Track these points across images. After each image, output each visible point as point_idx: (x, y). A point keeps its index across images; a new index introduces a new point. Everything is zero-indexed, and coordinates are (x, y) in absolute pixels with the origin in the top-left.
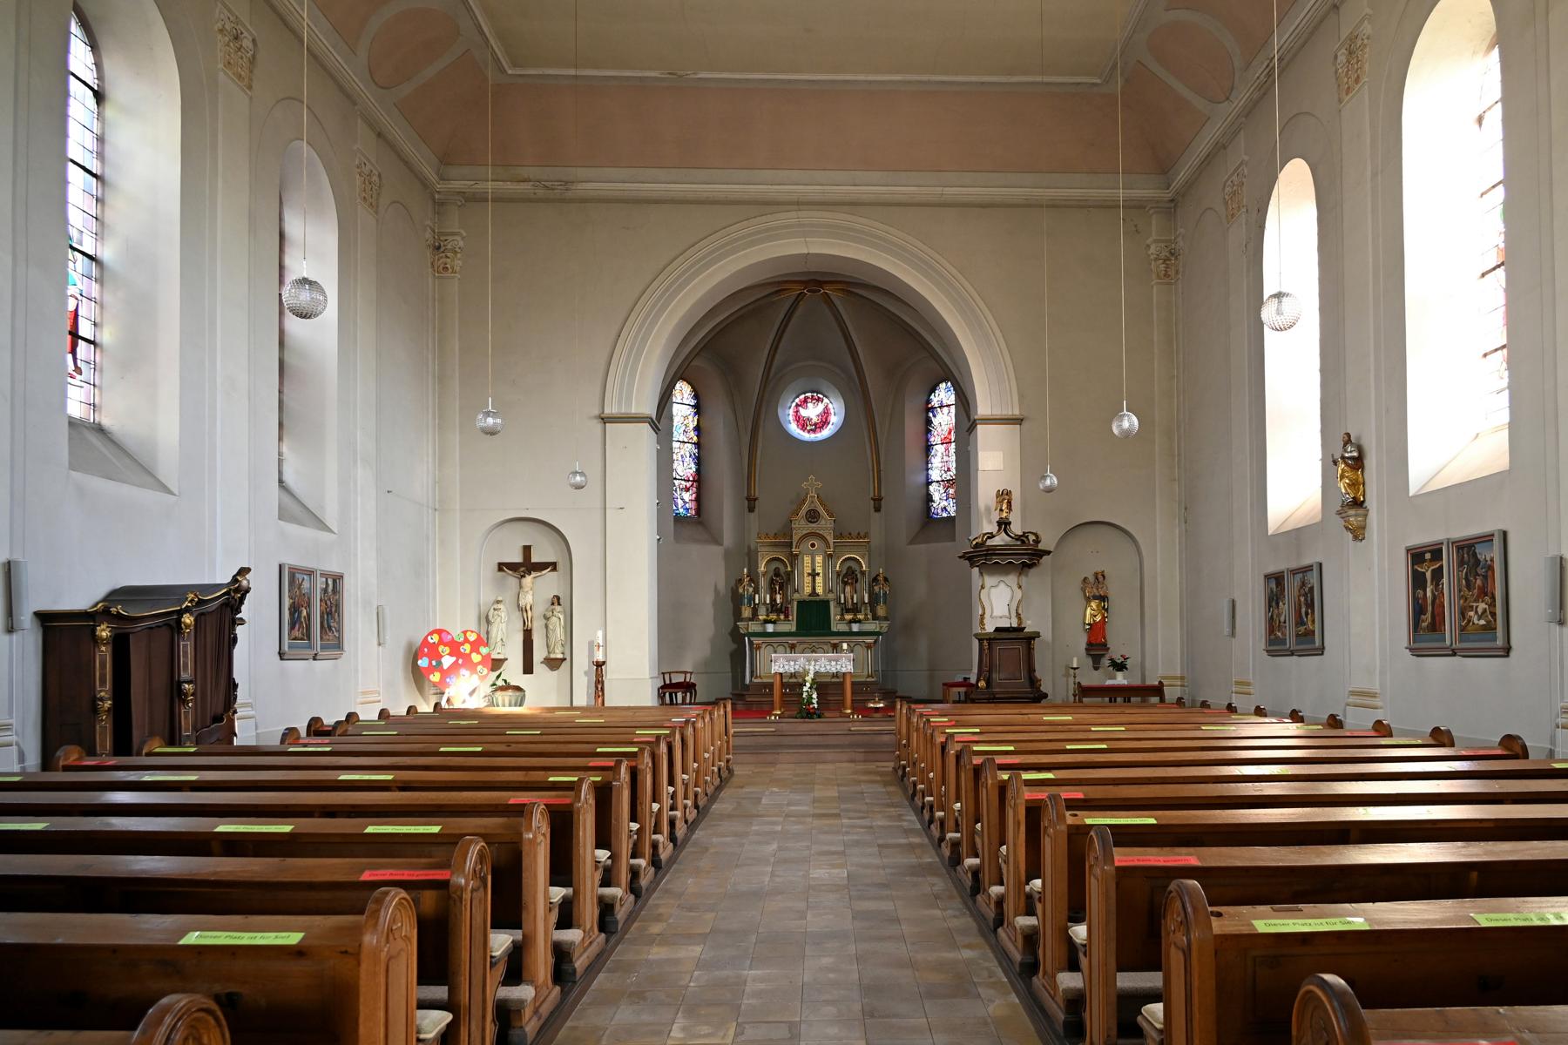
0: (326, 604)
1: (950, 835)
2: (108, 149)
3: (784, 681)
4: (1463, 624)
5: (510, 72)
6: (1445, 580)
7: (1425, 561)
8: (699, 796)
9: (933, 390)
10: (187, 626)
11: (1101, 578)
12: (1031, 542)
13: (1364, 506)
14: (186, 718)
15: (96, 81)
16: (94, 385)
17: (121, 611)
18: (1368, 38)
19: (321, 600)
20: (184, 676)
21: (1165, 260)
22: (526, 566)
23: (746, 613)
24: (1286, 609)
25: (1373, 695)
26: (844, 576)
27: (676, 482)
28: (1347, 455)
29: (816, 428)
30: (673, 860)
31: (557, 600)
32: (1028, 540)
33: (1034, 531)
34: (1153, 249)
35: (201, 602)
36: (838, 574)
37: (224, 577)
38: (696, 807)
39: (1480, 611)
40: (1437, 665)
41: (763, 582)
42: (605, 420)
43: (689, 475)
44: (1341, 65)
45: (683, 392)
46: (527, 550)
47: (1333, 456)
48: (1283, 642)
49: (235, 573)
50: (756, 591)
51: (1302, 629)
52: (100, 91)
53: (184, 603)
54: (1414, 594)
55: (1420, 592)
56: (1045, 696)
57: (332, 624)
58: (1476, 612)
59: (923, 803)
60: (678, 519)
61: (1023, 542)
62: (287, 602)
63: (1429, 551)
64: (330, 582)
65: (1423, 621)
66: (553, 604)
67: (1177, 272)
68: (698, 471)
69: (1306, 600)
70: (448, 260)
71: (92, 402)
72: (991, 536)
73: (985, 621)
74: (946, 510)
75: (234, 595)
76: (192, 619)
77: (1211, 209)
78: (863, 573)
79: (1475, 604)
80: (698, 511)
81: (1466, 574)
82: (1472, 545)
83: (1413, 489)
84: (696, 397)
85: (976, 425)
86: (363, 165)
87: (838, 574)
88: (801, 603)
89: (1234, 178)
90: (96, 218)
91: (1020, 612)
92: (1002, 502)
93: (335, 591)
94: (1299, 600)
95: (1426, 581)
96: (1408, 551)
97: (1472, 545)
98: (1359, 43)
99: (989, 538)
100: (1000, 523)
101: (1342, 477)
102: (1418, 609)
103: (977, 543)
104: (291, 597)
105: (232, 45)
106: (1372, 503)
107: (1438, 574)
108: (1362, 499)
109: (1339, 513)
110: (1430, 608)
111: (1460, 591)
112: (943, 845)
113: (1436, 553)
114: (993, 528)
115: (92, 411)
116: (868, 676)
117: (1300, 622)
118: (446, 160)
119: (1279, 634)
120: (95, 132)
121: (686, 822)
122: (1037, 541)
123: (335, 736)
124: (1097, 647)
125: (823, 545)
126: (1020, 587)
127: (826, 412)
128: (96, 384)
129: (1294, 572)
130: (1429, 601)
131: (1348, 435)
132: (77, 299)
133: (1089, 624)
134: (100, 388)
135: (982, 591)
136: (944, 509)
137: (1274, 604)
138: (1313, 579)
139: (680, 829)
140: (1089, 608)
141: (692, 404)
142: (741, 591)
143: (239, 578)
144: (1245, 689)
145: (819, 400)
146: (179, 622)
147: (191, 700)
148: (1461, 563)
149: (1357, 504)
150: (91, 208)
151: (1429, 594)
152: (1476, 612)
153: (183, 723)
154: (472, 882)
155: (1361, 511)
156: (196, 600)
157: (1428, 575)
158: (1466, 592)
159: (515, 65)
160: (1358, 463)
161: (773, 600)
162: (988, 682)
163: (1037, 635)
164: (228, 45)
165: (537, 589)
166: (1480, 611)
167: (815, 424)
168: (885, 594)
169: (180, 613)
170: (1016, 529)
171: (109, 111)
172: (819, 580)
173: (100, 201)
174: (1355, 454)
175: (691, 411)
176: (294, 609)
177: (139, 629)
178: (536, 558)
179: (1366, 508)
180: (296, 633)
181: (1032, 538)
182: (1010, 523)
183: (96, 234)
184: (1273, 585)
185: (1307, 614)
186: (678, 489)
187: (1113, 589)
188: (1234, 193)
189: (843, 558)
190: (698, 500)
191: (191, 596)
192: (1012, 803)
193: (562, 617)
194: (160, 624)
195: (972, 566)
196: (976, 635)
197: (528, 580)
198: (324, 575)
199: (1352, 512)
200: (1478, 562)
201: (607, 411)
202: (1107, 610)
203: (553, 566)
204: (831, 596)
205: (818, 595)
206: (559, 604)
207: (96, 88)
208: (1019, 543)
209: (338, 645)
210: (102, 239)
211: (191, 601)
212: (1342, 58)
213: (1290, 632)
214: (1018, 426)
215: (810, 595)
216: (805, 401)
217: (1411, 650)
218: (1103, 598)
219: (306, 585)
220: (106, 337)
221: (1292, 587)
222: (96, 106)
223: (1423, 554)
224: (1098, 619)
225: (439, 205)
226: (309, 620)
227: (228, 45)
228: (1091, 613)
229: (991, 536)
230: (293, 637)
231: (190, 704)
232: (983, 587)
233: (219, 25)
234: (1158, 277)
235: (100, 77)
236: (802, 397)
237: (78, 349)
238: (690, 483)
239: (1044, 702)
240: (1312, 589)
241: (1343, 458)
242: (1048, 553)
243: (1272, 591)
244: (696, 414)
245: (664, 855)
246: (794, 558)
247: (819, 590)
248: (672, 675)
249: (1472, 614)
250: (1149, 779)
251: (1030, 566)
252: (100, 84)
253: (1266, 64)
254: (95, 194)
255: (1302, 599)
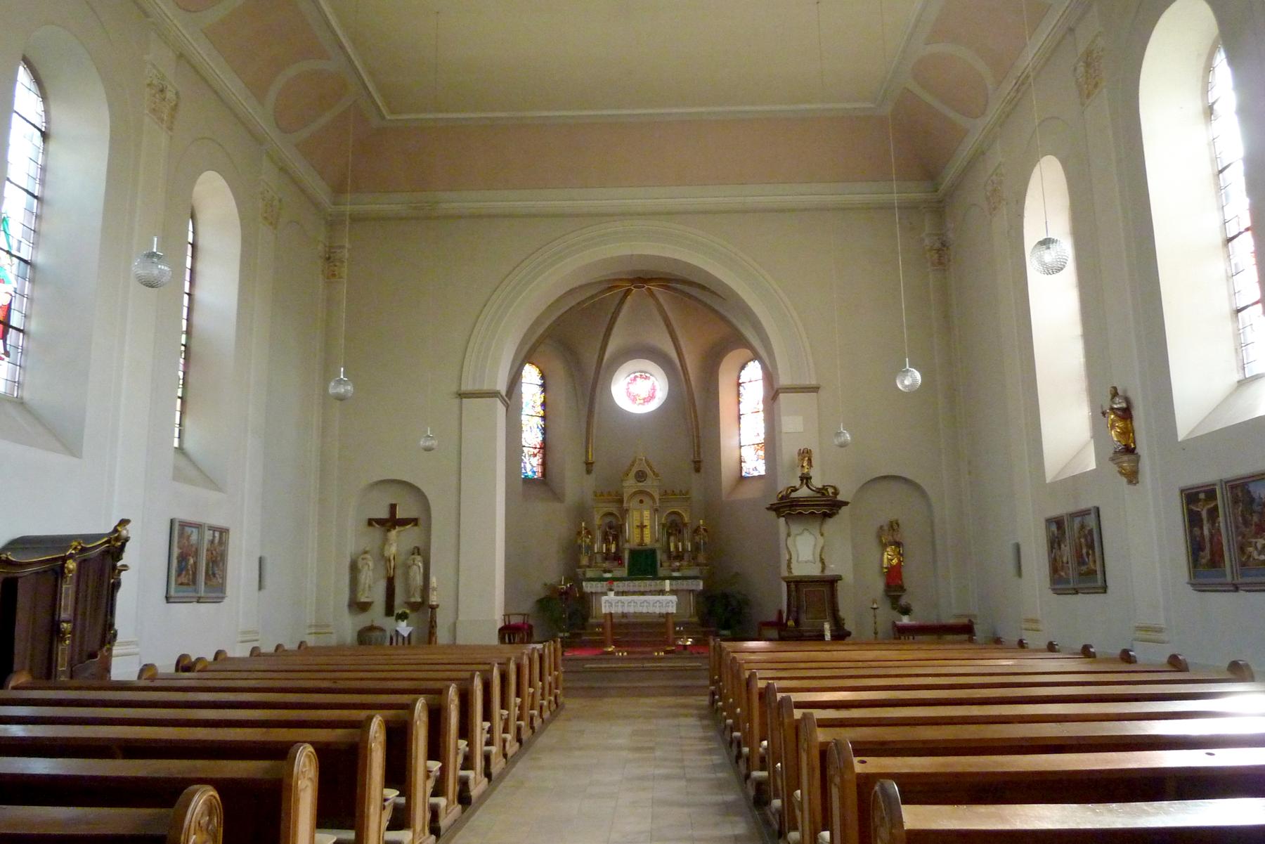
0: (212, 554)
1: (757, 774)
2: (49, 177)
3: (614, 620)
4: (1243, 559)
5: (389, 118)
6: (1221, 519)
7: (1199, 500)
8: (522, 729)
9: (743, 368)
10: (70, 571)
11: (895, 527)
12: (831, 495)
13: (1136, 452)
14: (63, 654)
15: (44, 124)
16: (20, 366)
17: (10, 557)
18: (1102, 51)
19: (207, 550)
20: (64, 616)
21: (939, 250)
22: (391, 522)
23: (585, 561)
24: (1067, 551)
25: (1160, 630)
26: (670, 527)
27: (524, 449)
28: (1115, 406)
29: (644, 402)
30: (484, 796)
31: (417, 551)
32: (828, 493)
33: (833, 485)
34: (927, 241)
35: (83, 550)
36: (664, 525)
37: (104, 526)
38: (519, 740)
39: (1259, 546)
40: (1221, 602)
41: (598, 535)
42: (462, 395)
43: (537, 443)
44: (1081, 75)
45: (531, 375)
46: (393, 508)
47: (1102, 406)
48: (1068, 582)
49: (116, 524)
50: (593, 541)
51: (1084, 568)
52: (47, 131)
53: (68, 550)
54: (1191, 532)
55: (1196, 530)
56: (849, 634)
57: (216, 572)
58: (1256, 548)
59: (731, 738)
60: (528, 481)
61: (823, 494)
62: (176, 552)
63: (1205, 492)
64: (217, 534)
65: (1203, 558)
66: (413, 554)
67: (949, 261)
68: (544, 440)
69: (1086, 540)
70: (336, 268)
71: (17, 380)
72: (795, 489)
73: (792, 566)
74: (756, 470)
75: (114, 546)
76: (75, 564)
77: (975, 205)
78: (685, 525)
79: (1254, 540)
80: (544, 474)
81: (1242, 511)
82: (1246, 484)
83: (1183, 433)
84: (543, 377)
85: (778, 395)
86: (266, 192)
87: (664, 525)
88: (633, 553)
89: (994, 177)
90: (34, 231)
91: (823, 557)
92: (803, 460)
93: (221, 542)
94: (1080, 542)
95: (1201, 520)
96: (1182, 491)
97: (1246, 484)
98: (1094, 56)
99: (792, 491)
100: (802, 479)
101: (1113, 427)
102: (1196, 548)
103: (782, 496)
104: (180, 548)
105: (157, 95)
106: (1142, 448)
107: (1213, 513)
108: (1133, 446)
109: (1112, 459)
110: (1208, 546)
111: (1237, 527)
112: (748, 781)
113: (1210, 493)
114: (797, 483)
115: (16, 388)
116: (690, 617)
117: (1081, 561)
118: (338, 189)
119: (1063, 574)
120: (40, 163)
121: (505, 756)
122: (836, 493)
123: (193, 672)
124: (894, 583)
125: (651, 502)
126: (822, 535)
127: (654, 389)
128: (22, 364)
129: (1073, 515)
130: (1207, 539)
131: (1115, 388)
132: (11, 295)
133: (886, 568)
134: (25, 371)
135: (789, 538)
136: (755, 469)
137: (1056, 546)
138: (1091, 522)
139: (496, 764)
140: (886, 553)
141: (540, 384)
142: (579, 541)
143: (119, 529)
144: (1034, 626)
145: (646, 378)
146: (63, 567)
147: (69, 637)
148: (1236, 501)
149: (1129, 450)
150: (30, 223)
151: (1206, 532)
152: (1256, 548)
153: (59, 659)
154: (194, 837)
155: (1132, 457)
156: (79, 547)
157: (1204, 514)
158: (1243, 529)
159: (392, 112)
160: (1126, 414)
161: (608, 550)
162: (797, 622)
163: (838, 578)
164: (154, 96)
165: (398, 543)
166: (1259, 546)
167: (644, 399)
168: (705, 543)
169: (64, 559)
170: (817, 482)
171: (53, 145)
172: (647, 531)
173: (38, 217)
174: (1124, 405)
175: (539, 390)
176: (183, 558)
177: (27, 573)
178: (400, 514)
179: (1137, 454)
180: (183, 579)
181: (831, 490)
182: (811, 478)
183: (33, 244)
184: (1054, 528)
185: (1088, 554)
186: (527, 456)
187: (906, 535)
188: (995, 190)
189: (670, 511)
190: (544, 464)
191: (75, 544)
192: (805, 746)
193: (420, 564)
194: (47, 569)
195: (779, 516)
196: (784, 579)
197: (393, 533)
198: (213, 529)
199: (1125, 458)
200: (1252, 500)
201: (464, 388)
202: (902, 555)
203: (415, 521)
204: (657, 545)
205: (646, 545)
206: (419, 554)
207: (43, 130)
208: (819, 495)
209: (221, 588)
210: (37, 247)
211: (75, 549)
212: (1081, 69)
213: (1071, 572)
214: (815, 394)
215: (639, 545)
216: (636, 377)
217: (1193, 585)
218: (898, 544)
219: (194, 538)
220: (33, 327)
221: (1072, 530)
222: (42, 144)
223: (1198, 493)
224: (895, 562)
225: (333, 223)
226: (196, 568)
227: (154, 96)
228: (889, 557)
229: (795, 489)
230: (180, 582)
231: (67, 642)
232: (789, 535)
233: (148, 81)
234: (933, 264)
235: (47, 121)
236: (632, 376)
237: (8, 336)
238: (538, 450)
239: (848, 640)
240: (1091, 532)
241: (1112, 409)
242: (846, 504)
243: (1053, 534)
244: (542, 392)
245: (475, 792)
246: (624, 512)
247: (647, 540)
248: (511, 617)
249: (1251, 549)
250: (951, 718)
251: (830, 516)
252: (47, 126)
253: (1014, 82)
254: (35, 211)
255: (1083, 540)
